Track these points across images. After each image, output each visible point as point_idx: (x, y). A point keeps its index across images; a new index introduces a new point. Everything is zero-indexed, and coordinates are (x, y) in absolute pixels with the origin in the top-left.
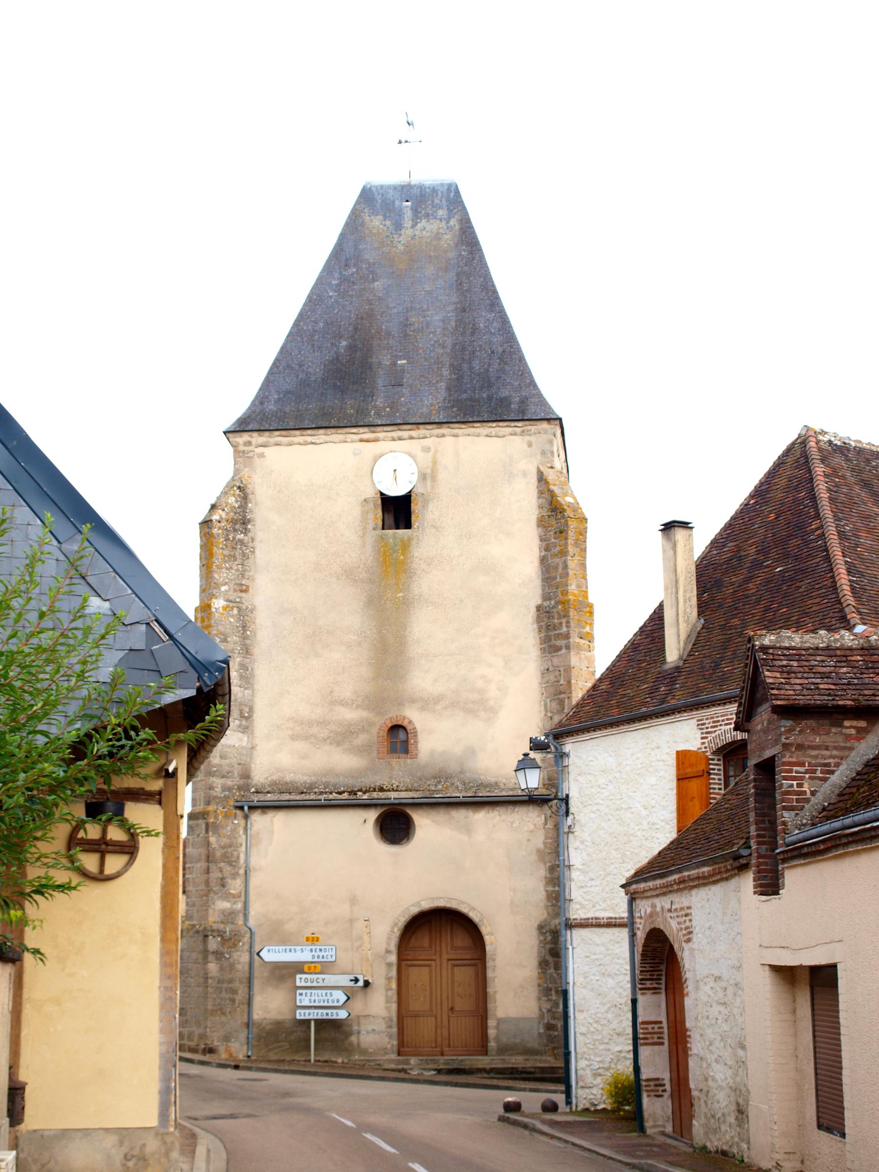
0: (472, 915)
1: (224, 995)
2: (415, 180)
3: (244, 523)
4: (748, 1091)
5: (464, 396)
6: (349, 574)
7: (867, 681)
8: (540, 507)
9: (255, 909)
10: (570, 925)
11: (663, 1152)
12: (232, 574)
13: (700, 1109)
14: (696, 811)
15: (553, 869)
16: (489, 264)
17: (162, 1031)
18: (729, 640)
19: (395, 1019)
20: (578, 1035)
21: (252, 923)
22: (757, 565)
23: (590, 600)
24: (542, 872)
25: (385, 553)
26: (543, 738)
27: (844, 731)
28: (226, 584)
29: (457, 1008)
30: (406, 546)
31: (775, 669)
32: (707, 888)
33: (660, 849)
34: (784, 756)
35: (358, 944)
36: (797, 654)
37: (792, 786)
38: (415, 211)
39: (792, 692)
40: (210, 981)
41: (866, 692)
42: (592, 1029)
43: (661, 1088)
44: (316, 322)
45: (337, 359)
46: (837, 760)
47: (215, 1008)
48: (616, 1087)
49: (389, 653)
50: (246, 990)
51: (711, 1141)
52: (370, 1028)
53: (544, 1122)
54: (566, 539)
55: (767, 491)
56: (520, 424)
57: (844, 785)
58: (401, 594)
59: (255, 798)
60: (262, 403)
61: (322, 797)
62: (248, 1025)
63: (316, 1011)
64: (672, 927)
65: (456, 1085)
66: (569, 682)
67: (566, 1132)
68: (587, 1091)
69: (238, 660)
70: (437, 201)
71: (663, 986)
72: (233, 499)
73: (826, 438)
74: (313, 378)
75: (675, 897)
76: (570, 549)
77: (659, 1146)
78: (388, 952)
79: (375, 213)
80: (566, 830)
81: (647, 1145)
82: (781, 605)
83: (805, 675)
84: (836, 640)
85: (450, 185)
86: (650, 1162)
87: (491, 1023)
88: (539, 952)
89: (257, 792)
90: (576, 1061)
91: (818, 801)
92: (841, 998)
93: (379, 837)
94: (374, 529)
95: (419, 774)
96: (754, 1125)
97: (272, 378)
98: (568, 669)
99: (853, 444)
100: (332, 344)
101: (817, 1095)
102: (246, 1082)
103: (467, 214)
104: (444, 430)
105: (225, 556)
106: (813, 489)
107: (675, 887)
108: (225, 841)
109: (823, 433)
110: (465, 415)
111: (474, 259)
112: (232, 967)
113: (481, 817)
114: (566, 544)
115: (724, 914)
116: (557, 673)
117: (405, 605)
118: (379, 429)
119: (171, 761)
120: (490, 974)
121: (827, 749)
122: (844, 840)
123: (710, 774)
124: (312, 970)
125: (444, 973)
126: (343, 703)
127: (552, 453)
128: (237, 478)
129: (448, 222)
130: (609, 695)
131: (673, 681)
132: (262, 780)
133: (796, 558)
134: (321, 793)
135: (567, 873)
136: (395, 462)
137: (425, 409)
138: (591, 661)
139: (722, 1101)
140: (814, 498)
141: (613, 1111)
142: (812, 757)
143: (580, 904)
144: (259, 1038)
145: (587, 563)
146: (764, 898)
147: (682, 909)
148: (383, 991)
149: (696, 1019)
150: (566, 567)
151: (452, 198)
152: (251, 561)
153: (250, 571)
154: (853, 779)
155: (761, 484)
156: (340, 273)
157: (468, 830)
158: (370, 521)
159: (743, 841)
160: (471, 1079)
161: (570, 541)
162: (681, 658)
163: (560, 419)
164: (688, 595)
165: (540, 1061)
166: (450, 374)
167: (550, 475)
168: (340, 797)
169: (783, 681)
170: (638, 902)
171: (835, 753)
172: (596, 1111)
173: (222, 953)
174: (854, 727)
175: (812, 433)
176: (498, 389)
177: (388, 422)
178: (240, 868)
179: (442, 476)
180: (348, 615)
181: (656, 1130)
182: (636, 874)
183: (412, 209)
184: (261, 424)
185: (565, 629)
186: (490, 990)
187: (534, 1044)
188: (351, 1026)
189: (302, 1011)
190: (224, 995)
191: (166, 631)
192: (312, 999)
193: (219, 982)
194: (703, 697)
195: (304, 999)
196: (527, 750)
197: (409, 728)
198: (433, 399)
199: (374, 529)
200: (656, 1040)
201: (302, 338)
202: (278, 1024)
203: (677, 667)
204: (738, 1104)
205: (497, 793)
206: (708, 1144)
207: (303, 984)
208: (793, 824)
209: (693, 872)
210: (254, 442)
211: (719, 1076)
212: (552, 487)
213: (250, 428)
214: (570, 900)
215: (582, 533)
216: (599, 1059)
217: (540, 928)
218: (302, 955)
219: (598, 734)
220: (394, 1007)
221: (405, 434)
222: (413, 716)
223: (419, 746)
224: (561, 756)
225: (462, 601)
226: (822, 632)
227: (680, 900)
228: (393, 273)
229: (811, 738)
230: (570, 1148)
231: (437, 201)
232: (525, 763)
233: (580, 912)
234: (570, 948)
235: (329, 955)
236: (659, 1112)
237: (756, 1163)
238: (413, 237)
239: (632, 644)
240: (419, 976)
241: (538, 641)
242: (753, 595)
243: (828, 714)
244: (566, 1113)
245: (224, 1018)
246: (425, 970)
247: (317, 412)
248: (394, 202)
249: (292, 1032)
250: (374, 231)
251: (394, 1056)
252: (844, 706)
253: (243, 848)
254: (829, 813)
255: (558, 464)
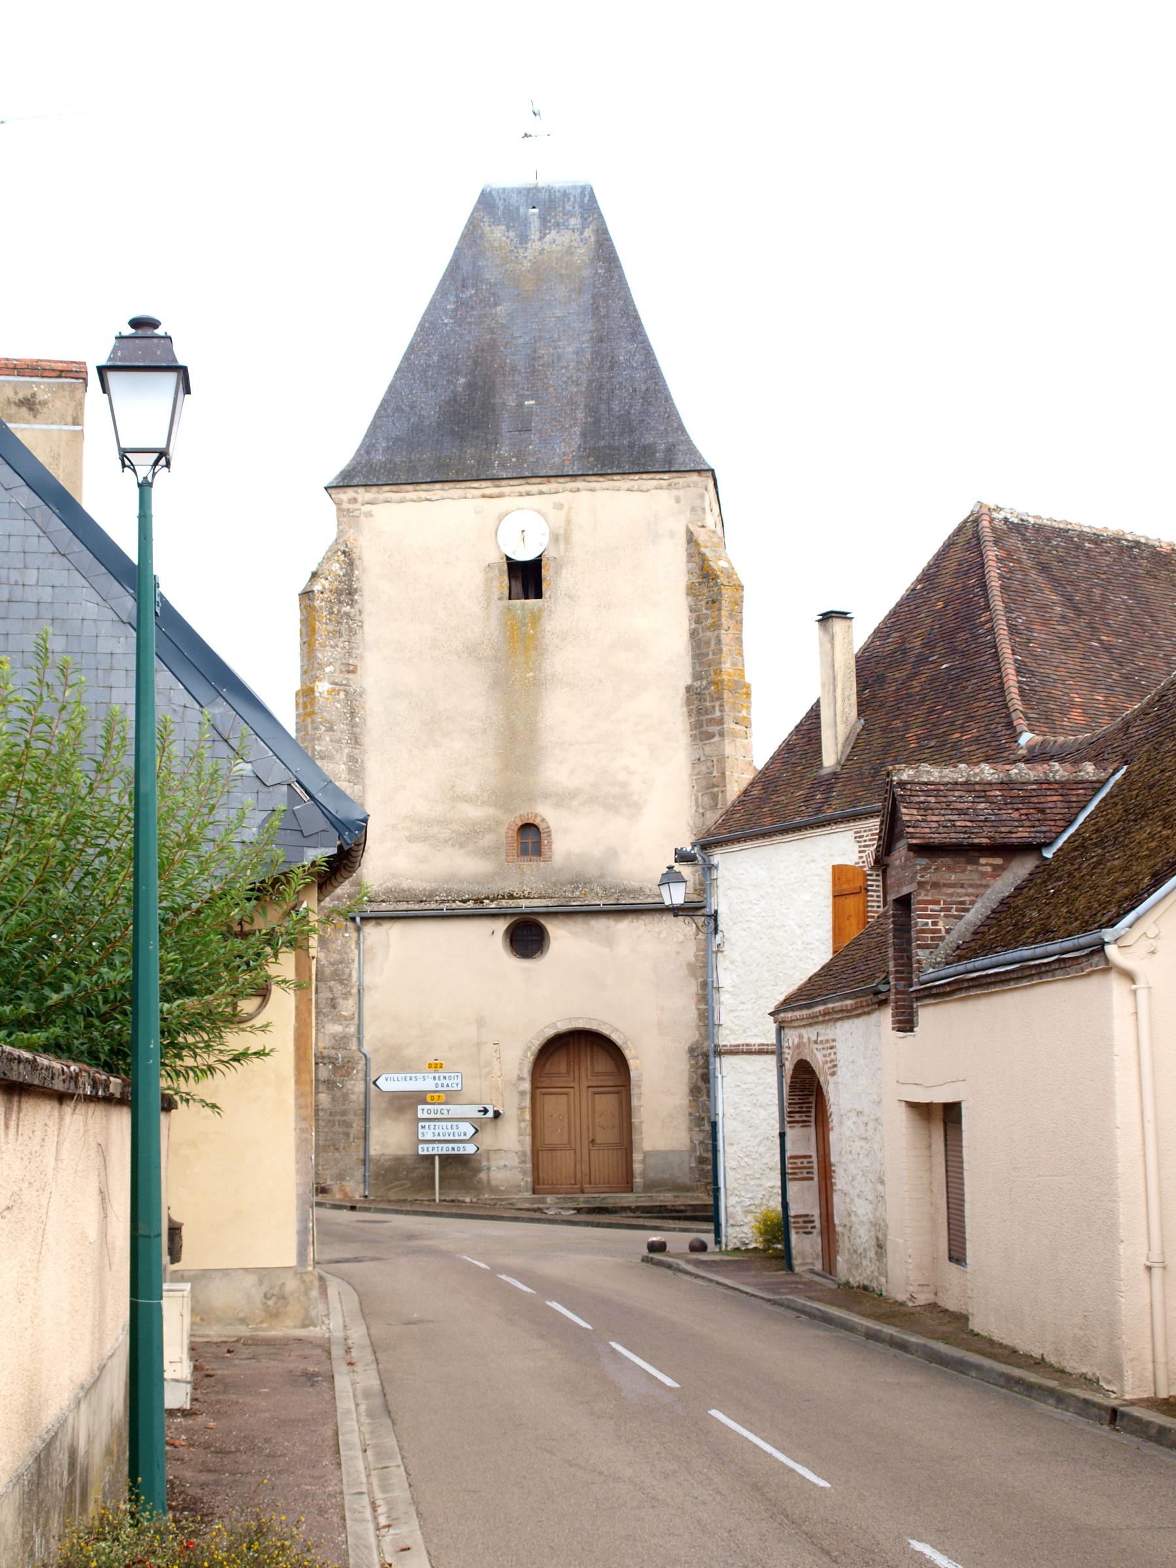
0: (614, 1037)
1: (336, 1128)
2: (542, 183)
3: (350, 594)
4: (886, 1226)
5: (602, 443)
6: (471, 651)
7: (1004, 817)
8: (690, 572)
9: (368, 1035)
10: (719, 1052)
11: (808, 1289)
12: (338, 653)
13: (844, 1244)
14: (853, 931)
15: (704, 985)
16: (630, 285)
17: (298, 1172)
18: (890, 744)
19: (529, 1153)
20: (728, 1170)
21: (366, 1048)
22: (922, 660)
23: (747, 680)
24: (693, 988)
25: (512, 626)
26: (689, 849)
27: (980, 868)
28: (331, 664)
29: (598, 1141)
30: (536, 618)
31: (912, 805)
32: (850, 1021)
33: (811, 974)
34: (919, 894)
35: (487, 1070)
36: (936, 789)
37: (927, 924)
38: (544, 219)
39: (927, 830)
40: (321, 1114)
41: (1003, 829)
42: (743, 1164)
43: (810, 1225)
44: (428, 355)
45: (455, 400)
46: (972, 898)
47: (327, 1143)
48: (765, 1224)
49: (518, 740)
50: (362, 1122)
51: (854, 1277)
52: (502, 1163)
53: (688, 1261)
54: (719, 610)
55: (936, 575)
56: (666, 476)
57: (979, 923)
58: (531, 674)
59: (368, 908)
60: (368, 453)
61: (444, 906)
62: (364, 1162)
63: (440, 1146)
64: (818, 1059)
65: (598, 1225)
66: (723, 774)
67: (711, 1271)
68: (737, 1229)
69: (346, 751)
70: (569, 208)
71: (813, 1119)
72: (337, 565)
73: (1001, 515)
74: (427, 423)
75: (820, 1029)
76: (724, 621)
77: (805, 1284)
78: (520, 1079)
79: (496, 222)
80: (715, 949)
81: (793, 1283)
82: (945, 706)
83: (943, 812)
84: (976, 775)
85: (584, 188)
86: (790, 1297)
87: (637, 1157)
88: (690, 1078)
89: (370, 901)
90: (726, 1198)
91: (953, 939)
92: (965, 1135)
93: (509, 949)
94: (499, 599)
95: (553, 879)
96: (892, 1259)
97: (379, 422)
98: (722, 759)
99: (1032, 521)
100: (448, 381)
101: (949, 1229)
102: (366, 1225)
103: (603, 223)
104: (580, 484)
105: (329, 632)
106: (984, 576)
107: (821, 1019)
108: (336, 957)
109: (998, 509)
110: (603, 466)
111: (612, 278)
112: (345, 1097)
113: (624, 926)
114: (720, 615)
115: (866, 1048)
116: (710, 764)
117: (536, 687)
118: (504, 483)
119: (302, 902)
120: (635, 1102)
121: (962, 886)
122: (966, 985)
123: (868, 891)
124: (436, 1100)
125: (584, 1103)
126: (466, 799)
127: (704, 509)
128: (340, 541)
129: (581, 233)
130: (762, 801)
131: (830, 789)
132: (375, 888)
133: (964, 654)
134: (443, 901)
135: (716, 996)
136: (522, 520)
137: (557, 460)
138: (747, 750)
139: (863, 1236)
140: (984, 586)
141: (765, 1250)
142: (947, 895)
143: (730, 1030)
144: (377, 1176)
145: (744, 637)
146: (901, 1034)
147: (827, 1041)
148: (515, 1123)
149: (840, 1153)
150: (719, 642)
151: (587, 205)
152: (358, 637)
153: (357, 649)
154: (988, 918)
155: (929, 567)
156: (457, 296)
157: (609, 942)
158: (495, 590)
159: (883, 976)
160: (613, 1219)
161: (723, 613)
162: (838, 763)
163: (713, 471)
164: (847, 693)
165: (692, 1198)
166: (586, 417)
167: (701, 536)
168: (465, 905)
169: (919, 818)
170: (786, 1031)
171: (970, 890)
172: (747, 1250)
173: (335, 1082)
174: (991, 865)
175: (985, 510)
176: (641, 434)
177: (515, 475)
178: (352, 987)
179: (577, 537)
180: (471, 698)
181: (805, 1268)
182: (785, 1002)
183: (539, 217)
184: (367, 478)
185: (718, 714)
186: (635, 1120)
187: (686, 1180)
188: (479, 1161)
189: (425, 1146)
190: (336, 1128)
191: (307, 791)
192: (436, 1132)
193: (331, 1114)
194: (861, 808)
195: (427, 1133)
196: (672, 863)
197: (541, 827)
198: (566, 447)
199: (499, 599)
200: (805, 1175)
201: (413, 375)
202: (398, 1160)
203: (835, 773)
204: (877, 1238)
205: (641, 899)
206: (851, 1280)
207: (426, 1116)
208: (928, 964)
209: (837, 1005)
210: (360, 500)
211: (861, 1211)
212: (703, 550)
213: (355, 482)
214: (720, 1025)
215: (738, 602)
216: (750, 1195)
217: (691, 1050)
218: (423, 1083)
219: (749, 844)
220: (528, 1140)
221: (534, 489)
222: (547, 814)
223: (554, 846)
224: (710, 868)
225: (600, 681)
226: (962, 766)
227: (826, 1032)
228: (519, 295)
229: (947, 876)
230: (713, 1285)
231: (569, 208)
232: (670, 877)
233: (730, 1038)
234: (720, 1076)
235: (454, 1083)
236: (808, 1249)
237: (893, 1295)
238: (542, 252)
239: (787, 744)
240: (555, 1105)
241: (688, 727)
242: (917, 694)
243: (965, 852)
244: (714, 1253)
245: (337, 1155)
246: (564, 1098)
247: (432, 462)
248: (518, 209)
249: (414, 1169)
250: (496, 244)
251: (528, 1195)
252: (980, 845)
253: (356, 965)
254: (964, 952)
255: (711, 520)
